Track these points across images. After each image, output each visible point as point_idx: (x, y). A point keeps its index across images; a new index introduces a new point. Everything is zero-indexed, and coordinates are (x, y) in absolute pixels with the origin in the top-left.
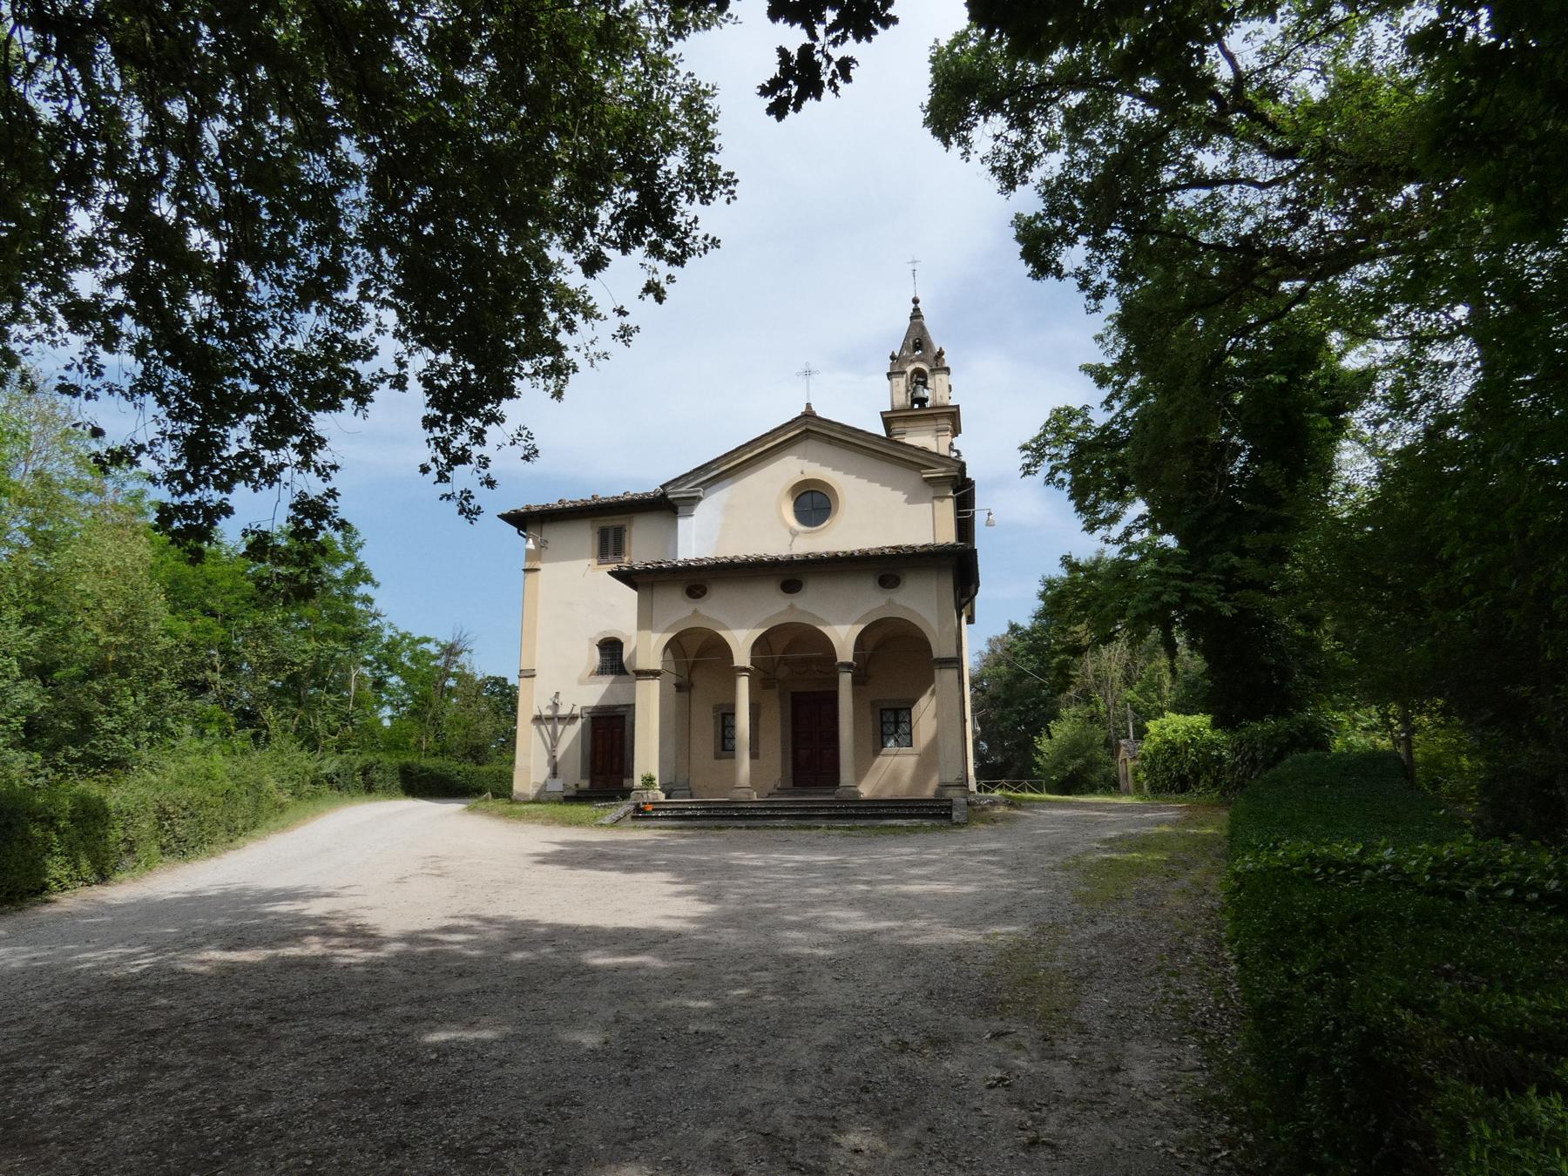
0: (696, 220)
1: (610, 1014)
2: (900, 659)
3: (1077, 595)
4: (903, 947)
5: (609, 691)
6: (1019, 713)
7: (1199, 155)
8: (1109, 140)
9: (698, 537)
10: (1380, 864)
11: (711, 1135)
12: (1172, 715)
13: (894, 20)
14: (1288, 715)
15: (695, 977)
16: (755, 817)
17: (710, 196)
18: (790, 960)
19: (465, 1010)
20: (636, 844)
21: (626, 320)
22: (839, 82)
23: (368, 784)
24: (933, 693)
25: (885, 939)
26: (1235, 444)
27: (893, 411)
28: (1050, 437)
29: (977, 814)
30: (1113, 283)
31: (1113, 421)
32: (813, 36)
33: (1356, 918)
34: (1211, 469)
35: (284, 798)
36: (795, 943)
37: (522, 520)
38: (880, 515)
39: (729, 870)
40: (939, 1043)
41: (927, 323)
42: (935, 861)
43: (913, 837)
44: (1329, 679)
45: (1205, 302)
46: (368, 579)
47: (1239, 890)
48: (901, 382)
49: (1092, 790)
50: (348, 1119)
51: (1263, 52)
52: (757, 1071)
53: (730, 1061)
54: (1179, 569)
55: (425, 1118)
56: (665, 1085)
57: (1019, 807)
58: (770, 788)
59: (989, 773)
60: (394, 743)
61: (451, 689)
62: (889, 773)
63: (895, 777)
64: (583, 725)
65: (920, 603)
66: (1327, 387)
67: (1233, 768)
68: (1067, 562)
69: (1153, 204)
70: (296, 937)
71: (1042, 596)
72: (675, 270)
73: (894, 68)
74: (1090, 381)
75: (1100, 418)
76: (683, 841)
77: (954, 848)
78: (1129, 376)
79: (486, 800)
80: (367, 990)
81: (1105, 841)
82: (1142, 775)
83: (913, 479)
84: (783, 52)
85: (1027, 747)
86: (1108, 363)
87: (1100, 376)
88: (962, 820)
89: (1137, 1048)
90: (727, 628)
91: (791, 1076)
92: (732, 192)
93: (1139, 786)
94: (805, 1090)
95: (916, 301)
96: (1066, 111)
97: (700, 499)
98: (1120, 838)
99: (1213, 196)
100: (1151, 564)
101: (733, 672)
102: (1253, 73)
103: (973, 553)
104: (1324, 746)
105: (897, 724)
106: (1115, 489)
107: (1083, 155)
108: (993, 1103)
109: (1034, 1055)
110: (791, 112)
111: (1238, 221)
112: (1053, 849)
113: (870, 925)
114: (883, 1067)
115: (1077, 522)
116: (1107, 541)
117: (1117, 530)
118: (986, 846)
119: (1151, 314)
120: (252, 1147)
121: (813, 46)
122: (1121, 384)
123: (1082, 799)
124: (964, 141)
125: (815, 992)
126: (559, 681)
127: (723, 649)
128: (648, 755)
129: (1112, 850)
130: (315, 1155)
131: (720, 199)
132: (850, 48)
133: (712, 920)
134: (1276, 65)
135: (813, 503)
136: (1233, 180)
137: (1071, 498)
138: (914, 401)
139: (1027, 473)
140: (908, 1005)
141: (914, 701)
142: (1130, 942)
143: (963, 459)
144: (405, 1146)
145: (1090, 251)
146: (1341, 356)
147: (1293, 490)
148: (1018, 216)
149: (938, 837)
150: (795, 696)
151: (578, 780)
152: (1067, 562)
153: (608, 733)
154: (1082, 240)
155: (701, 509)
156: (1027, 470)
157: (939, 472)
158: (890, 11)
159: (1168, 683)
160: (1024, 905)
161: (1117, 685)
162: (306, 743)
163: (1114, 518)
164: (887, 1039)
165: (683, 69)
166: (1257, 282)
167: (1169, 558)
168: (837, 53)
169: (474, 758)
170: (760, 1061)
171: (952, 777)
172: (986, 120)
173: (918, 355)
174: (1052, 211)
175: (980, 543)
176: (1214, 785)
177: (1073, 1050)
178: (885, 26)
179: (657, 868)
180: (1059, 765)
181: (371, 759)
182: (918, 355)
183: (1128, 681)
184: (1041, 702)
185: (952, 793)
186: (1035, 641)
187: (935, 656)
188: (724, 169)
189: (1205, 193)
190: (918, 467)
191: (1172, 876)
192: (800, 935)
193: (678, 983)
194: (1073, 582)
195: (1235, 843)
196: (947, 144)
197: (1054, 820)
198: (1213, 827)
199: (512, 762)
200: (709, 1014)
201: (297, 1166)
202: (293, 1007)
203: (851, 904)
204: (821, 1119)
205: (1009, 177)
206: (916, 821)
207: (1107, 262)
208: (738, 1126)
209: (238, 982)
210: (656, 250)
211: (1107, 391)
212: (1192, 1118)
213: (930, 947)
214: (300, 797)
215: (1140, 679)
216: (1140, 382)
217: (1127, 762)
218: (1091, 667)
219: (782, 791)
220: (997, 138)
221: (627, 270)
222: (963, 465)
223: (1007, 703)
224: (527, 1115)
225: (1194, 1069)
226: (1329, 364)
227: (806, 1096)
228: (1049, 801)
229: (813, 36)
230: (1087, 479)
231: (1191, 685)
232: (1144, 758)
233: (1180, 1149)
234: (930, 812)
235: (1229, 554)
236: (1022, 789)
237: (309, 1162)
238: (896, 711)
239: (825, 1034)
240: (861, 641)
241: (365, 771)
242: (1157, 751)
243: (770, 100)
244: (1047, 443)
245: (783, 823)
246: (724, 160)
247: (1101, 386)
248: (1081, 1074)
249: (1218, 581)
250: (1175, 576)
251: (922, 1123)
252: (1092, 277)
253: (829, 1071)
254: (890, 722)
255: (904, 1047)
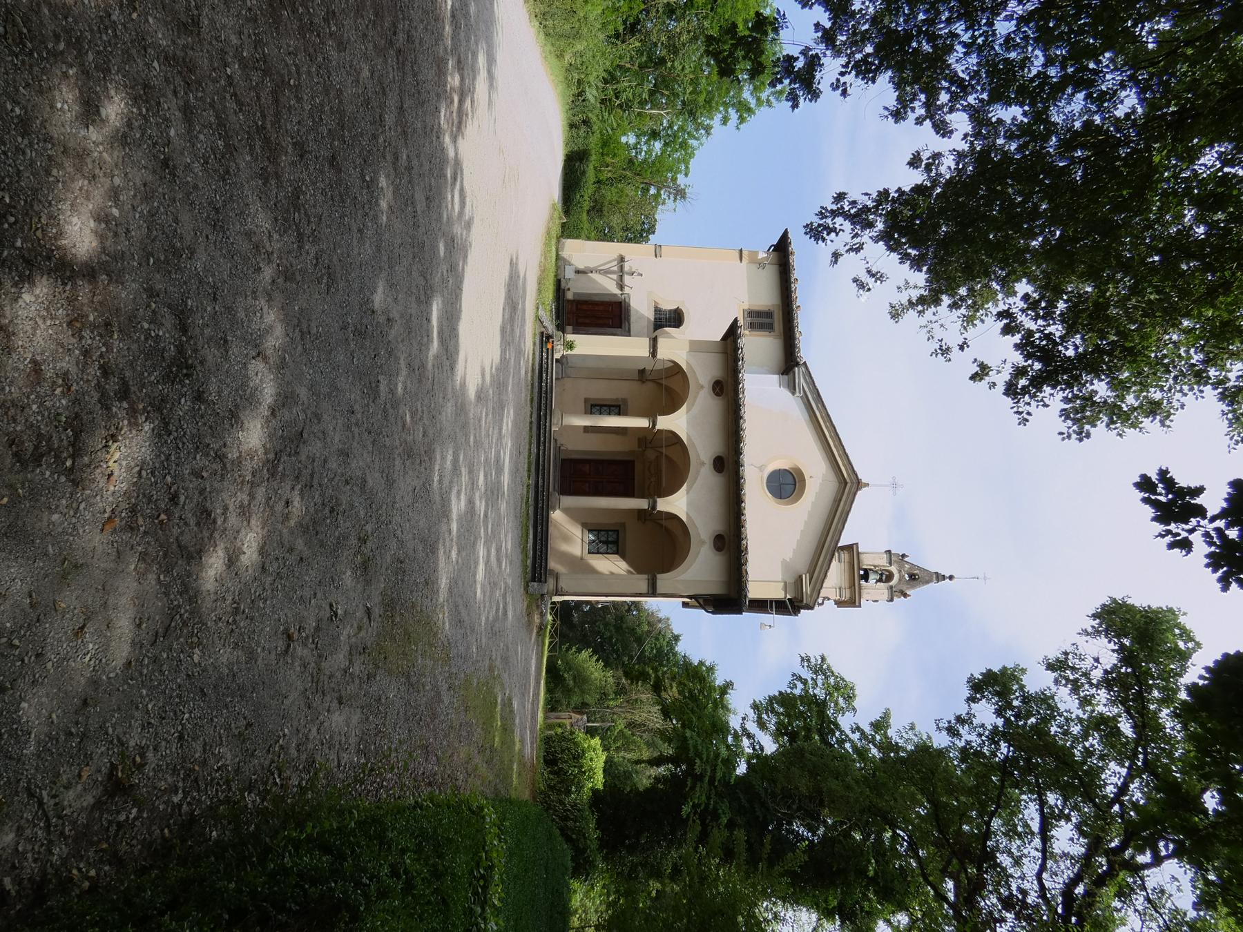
0: (1046, 405)
1: (395, 314)
2: (658, 547)
3: (701, 691)
4: (437, 541)
5: (642, 317)
6: (611, 637)
7: (1070, 826)
8: (1088, 753)
9: (761, 390)
10: (485, 919)
11: (303, 392)
12: (604, 758)
13: (1225, 588)
14: (601, 848)
15: (420, 381)
16: (539, 428)
17: (1067, 417)
18: (430, 453)
19: (404, 202)
20: (522, 335)
21: (956, 349)
22: (1169, 539)
23: (578, 124)
24: (629, 572)
25: (444, 528)
26: (818, 829)
27: (858, 553)
28: (832, 680)
29: (535, 601)
30: (961, 744)
31: (842, 732)
32: (1213, 519)
33: (444, 901)
34: (799, 809)
35: (568, 57)
36: (443, 458)
37: (782, 248)
38: (775, 541)
39: (500, 407)
40: (365, 569)
41: (932, 586)
42: (500, 567)
43: (519, 550)
44: (626, 883)
45: (939, 815)
46: (742, 120)
47: (470, 810)
48: (883, 561)
49: (549, 691)
50: (323, 112)
51: (1163, 892)
52: (349, 428)
53: (357, 407)
54: (719, 774)
55: (322, 172)
56: (341, 357)
57: (538, 634)
58: (561, 441)
59: (564, 611)
60: (607, 143)
61: (648, 190)
62: (569, 535)
63: (567, 539)
64: (615, 295)
65: (701, 567)
66: (862, 908)
67: (561, 802)
68: (728, 686)
69: (1029, 783)
70: (460, 66)
71: (701, 663)
72: (1001, 387)
73: (1178, 582)
74: (876, 716)
75: (845, 722)
76: (523, 372)
77: (510, 582)
78: (880, 748)
79: (560, 218)
80: (419, 125)
81: (510, 699)
82: (560, 730)
83: (802, 566)
84: (1199, 491)
85: (584, 642)
86: (891, 732)
87: (880, 725)
88: (530, 589)
89: (355, 719)
90: (688, 492)
91: (344, 454)
92: (1069, 437)
93: (550, 727)
94: (333, 464)
95: (951, 578)
96: (1115, 719)
97: (793, 394)
98: (512, 711)
99: (1033, 833)
100: (724, 752)
101: (652, 415)
102: (1142, 879)
103: (740, 612)
104: (576, 873)
105: (606, 543)
106: (786, 728)
107: (1076, 729)
108: (320, 607)
109: (354, 640)
110: (1142, 495)
111: (1010, 853)
112: (505, 660)
113: (454, 516)
114: (348, 524)
115: (761, 697)
116: (744, 719)
117: (752, 727)
118: (510, 608)
119: (932, 773)
120: (304, 37)
121: (1204, 517)
122: (873, 741)
123: (543, 682)
124: (1097, 632)
125: (405, 472)
126: (650, 274)
127: (672, 408)
128: (590, 345)
129: (504, 705)
130: (297, 87)
131: (1063, 426)
132: (1201, 549)
133: (463, 394)
134: (1148, 899)
135: (786, 485)
136: (1046, 853)
137: (781, 693)
138: (866, 571)
139: (803, 660)
140: (393, 544)
141: (623, 557)
142: (434, 716)
143: (816, 607)
144: (301, 156)
145: (990, 727)
146: (888, 922)
147: (782, 875)
148: (1023, 671)
149: (518, 570)
150: (633, 462)
151: (573, 290)
152: (728, 686)
153: (607, 315)
154: (1000, 722)
155: (786, 393)
156: (805, 660)
157: (807, 588)
158: (1234, 586)
159: (629, 756)
160: (465, 636)
161: (628, 715)
162: (610, 73)
163: (762, 725)
164: (369, 528)
165: (1189, 399)
166: (955, 861)
167: (728, 768)
168: (1196, 538)
169: (593, 208)
170: (356, 430)
171: (563, 584)
172: (1113, 651)
173: (906, 577)
174: (1026, 699)
175: (747, 617)
176: (549, 786)
177: (356, 669)
178: (1220, 580)
179: (503, 352)
180: (569, 666)
181: (595, 127)
182: (906, 577)
183: (631, 725)
184: (618, 656)
185: (551, 583)
186: (667, 655)
187: (659, 576)
188: (1092, 430)
189: (1035, 826)
190: (812, 573)
191: (481, 750)
192: (449, 462)
193: (417, 369)
194: (712, 689)
195: (504, 802)
196: (1095, 616)
197: (528, 661)
198: (520, 787)
199: (589, 239)
200: (392, 391)
201: (290, 73)
202: (408, 68)
203: (471, 502)
204: (312, 476)
205: (1058, 666)
206: (531, 553)
207: (979, 741)
208: (309, 412)
209: (428, 23)
210: (1020, 372)
211: (868, 730)
212: (304, 757)
213: (436, 562)
214: (568, 70)
215: (633, 734)
216: (874, 756)
217: (570, 720)
218: (644, 697)
219: (558, 450)
220: (1097, 660)
221: (1004, 353)
222: (812, 608)
223: (619, 629)
224: (322, 251)
225: (339, 761)
226: (881, 912)
227: (328, 466)
228: (542, 657)
229: (1213, 519)
230: (794, 706)
231: (628, 775)
232: (572, 733)
233: (281, 747)
234: (537, 563)
235: (729, 816)
236: (552, 637)
237: (292, 82)
238: (616, 542)
239: (375, 480)
240: (673, 517)
241: (586, 122)
242: (577, 744)
243: (1154, 478)
244: (827, 678)
245: (534, 450)
246: (1100, 431)
247: (872, 724)
248: (338, 674)
249: (707, 805)
250: (714, 771)
251: (306, 553)
252: (966, 727)
253: (347, 483)
254: (608, 538)
255: (363, 540)
